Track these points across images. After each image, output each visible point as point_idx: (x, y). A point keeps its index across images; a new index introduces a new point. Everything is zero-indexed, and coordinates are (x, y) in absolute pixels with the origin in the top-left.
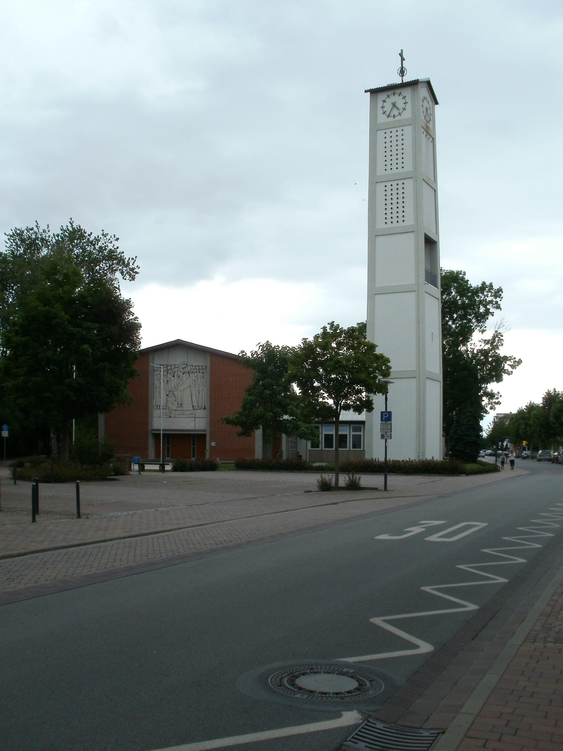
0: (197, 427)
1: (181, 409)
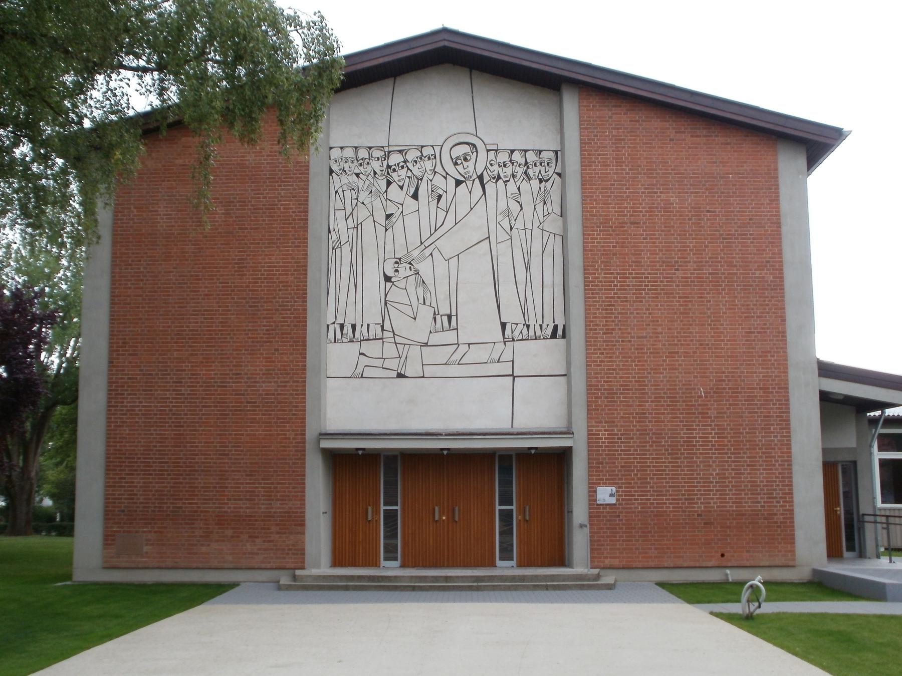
0: (523, 422)
1: (450, 337)
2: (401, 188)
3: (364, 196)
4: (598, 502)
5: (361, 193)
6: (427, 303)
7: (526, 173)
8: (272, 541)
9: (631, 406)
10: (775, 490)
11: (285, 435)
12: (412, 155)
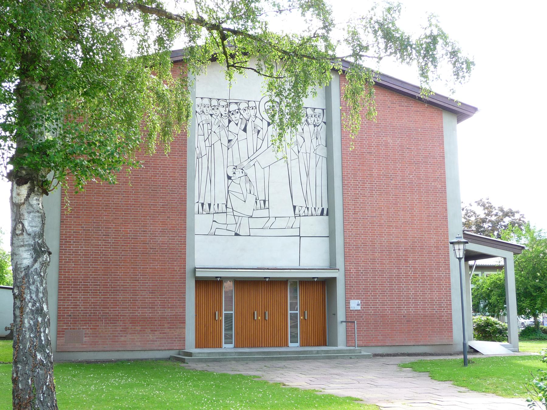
0: (305, 263)
1: (265, 213)
2: (237, 124)
3: (215, 128)
4: (351, 309)
5: (214, 126)
6: (252, 193)
7: (307, 121)
8: (166, 333)
9: (368, 255)
10: (443, 303)
11: (174, 268)
12: (243, 106)
